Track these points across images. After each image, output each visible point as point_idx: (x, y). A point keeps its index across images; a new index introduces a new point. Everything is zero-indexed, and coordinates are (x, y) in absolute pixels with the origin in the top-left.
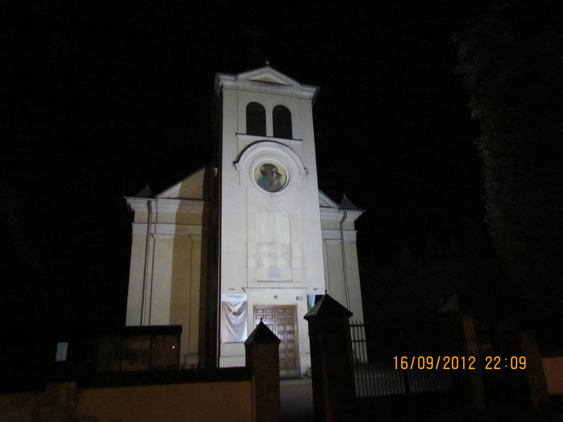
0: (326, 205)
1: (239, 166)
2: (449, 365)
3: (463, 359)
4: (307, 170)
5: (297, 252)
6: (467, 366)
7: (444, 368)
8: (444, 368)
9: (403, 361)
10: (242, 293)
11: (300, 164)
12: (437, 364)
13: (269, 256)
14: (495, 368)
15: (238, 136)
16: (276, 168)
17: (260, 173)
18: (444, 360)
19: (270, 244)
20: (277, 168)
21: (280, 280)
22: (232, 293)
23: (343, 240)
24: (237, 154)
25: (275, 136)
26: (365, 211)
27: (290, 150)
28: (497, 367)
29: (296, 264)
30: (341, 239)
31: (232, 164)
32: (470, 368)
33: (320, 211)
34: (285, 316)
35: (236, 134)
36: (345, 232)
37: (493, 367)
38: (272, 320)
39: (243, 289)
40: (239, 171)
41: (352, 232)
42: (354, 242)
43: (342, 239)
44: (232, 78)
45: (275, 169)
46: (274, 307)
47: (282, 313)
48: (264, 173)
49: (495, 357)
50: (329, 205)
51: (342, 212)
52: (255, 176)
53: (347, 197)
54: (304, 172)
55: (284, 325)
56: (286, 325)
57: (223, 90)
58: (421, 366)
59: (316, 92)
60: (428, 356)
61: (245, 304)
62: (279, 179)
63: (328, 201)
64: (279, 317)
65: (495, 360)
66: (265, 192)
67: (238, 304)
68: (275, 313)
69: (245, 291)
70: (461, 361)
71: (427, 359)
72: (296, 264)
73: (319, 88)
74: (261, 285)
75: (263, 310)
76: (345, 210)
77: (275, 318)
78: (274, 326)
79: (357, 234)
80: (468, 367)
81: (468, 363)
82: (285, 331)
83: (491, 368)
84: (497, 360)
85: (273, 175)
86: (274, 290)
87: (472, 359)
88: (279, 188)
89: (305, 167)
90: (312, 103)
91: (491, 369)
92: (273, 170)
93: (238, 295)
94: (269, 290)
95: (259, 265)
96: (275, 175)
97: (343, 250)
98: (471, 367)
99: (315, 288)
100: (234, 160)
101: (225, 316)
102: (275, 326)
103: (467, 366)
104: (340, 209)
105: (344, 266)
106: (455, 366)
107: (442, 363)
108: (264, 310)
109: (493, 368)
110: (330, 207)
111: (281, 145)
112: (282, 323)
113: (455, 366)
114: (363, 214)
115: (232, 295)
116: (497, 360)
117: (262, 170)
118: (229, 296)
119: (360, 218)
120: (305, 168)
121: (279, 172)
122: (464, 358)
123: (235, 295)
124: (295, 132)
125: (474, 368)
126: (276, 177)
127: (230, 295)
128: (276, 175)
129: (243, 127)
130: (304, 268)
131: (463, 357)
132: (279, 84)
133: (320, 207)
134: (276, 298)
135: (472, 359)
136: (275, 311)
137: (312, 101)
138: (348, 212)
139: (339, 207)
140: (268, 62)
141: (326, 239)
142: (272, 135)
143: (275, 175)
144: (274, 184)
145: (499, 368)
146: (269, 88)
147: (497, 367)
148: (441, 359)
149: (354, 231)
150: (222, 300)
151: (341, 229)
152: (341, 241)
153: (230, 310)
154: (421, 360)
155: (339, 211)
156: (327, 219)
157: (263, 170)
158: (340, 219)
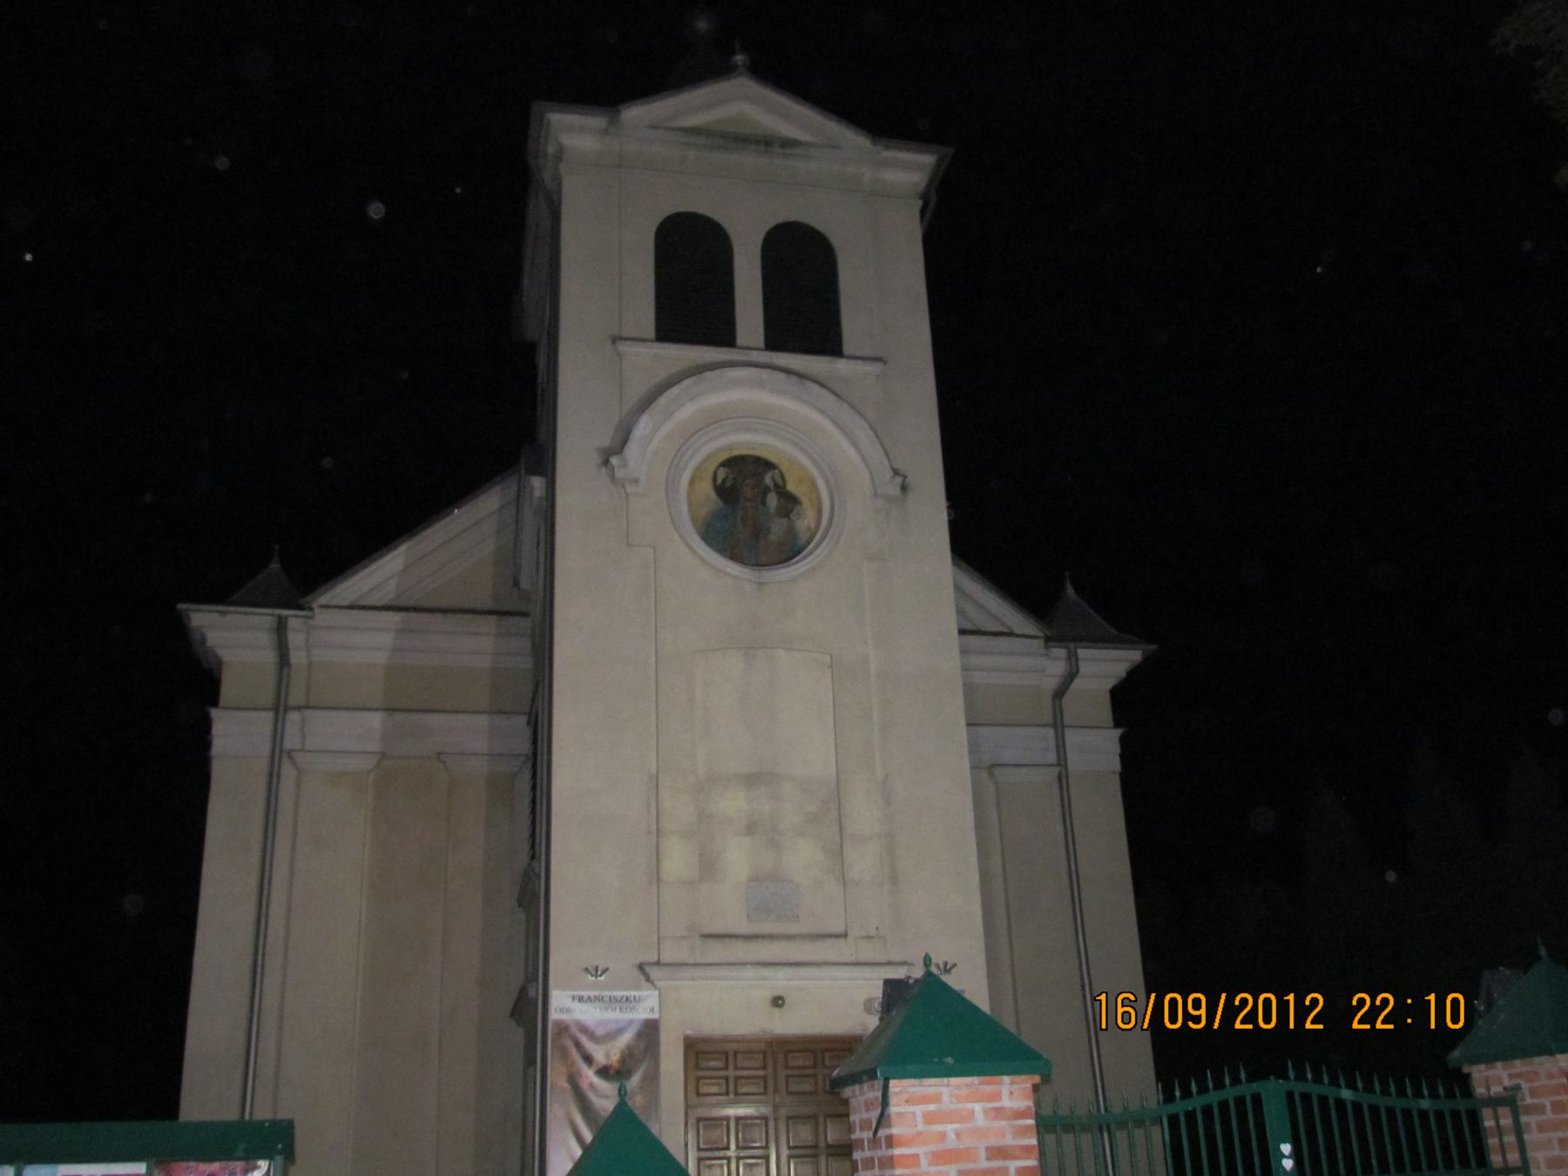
0: (991, 627)
1: (625, 464)
2: (1251, 1018)
3: (1288, 1001)
4: (905, 477)
5: (864, 814)
6: (1300, 1020)
7: (1238, 1025)
8: (1238, 1025)
9: (1123, 1006)
10: (637, 987)
11: (876, 454)
12: (1216, 1013)
13: (750, 829)
14: (1379, 1026)
15: (623, 347)
16: (776, 471)
17: (713, 495)
18: (1237, 1003)
19: (752, 780)
20: (781, 472)
21: (794, 929)
22: (594, 987)
23: (1066, 769)
24: (616, 420)
25: (776, 341)
26: (1153, 647)
27: (832, 398)
28: (1383, 1022)
29: (864, 862)
30: (1059, 765)
31: (596, 458)
32: (1308, 1026)
33: (964, 651)
34: (816, 1083)
35: (615, 339)
36: (1071, 737)
37: (1373, 1024)
38: (763, 1097)
39: (641, 967)
40: (623, 486)
41: (1101, 732)
42: (1114, 772)
43: (1063, 763)
44: (596, 121)
45: (773, 480)
46: (771, 1043)
47: (805, 1067)
48: (727, 492)
49: (1377, 996)
50: (1003, 624)
51: (1060, 652)
52: (690, 505)
53: (1077, 591)
54: (893, 490)
55: (814, 1117)
56: (821, 1119)
57: (563, 168)
58: (1173, 1020)
59: (938, 165)
60: (1192, 993)
61: (650, 1030)
62: (791, 515)
63: (995, 607)
64: (794, 1088)
65: (1378, 1003)
66: (734, 568)
67: (620, 1031)
68: (775, 1069)
69: (648, 979)
70: (1283, 1007)
71: (1190, 1000)
72: (864, 862)
73: (951, 151)
74: (717, 951)
75: (726, 1054)
76: (1071, 645)
77: (776, 1091)
78: (771, 1124)
79: (1124, 741)
80: (1305, 1023)
81: (1302, 1012)
82: (816, 1146)
83: (1368, 1027)
84: (1385, 1002)
85: (764, 503)
86: (767, 972)
87: (1315, 1002)
88: (790, 551)
89: (895, 466)
90: (923, 212)
91: (1367, 1030)
92: (763, 478)
93: (618, 994)
94: (750, 972)
95: (708, 867)
96: (772, 501)
97: (1067, 807)
98: (1312, 1023)
99: (946, 964)
100: (606, 441)
101: (564, 1084)
102: (777, 1130)
103: (1300, 1020)
104: (1049, 640)
105: (1074, 875)
106: (1267, 1020)
107: (1231, 1012)
108: (731, 1059)
109: (1373, 1025)
110: (1011, 634)
111: (795, 379)
112: (805, 1110)
113: (1267, 1020)
114: (1147, 660)
115: (597, 993)
116: (1385, 1002)
117: (719, 481)
118: (581, 999)
119: (1134, 675)
120: (896, 472)
121: (791, 487)
122: (1291, 997)
123: (607, 993)
124: (854, 326)
125: (1321, 1027)
126: (778, 508)
127: (585, 994)
128: (779, 500)
129: (642, 312)
130: (894, 880)
131: (1288, 994)
132: (788, 143)
133: (962, 632)
134: (781, 1006)
135: (1315, 1002)
136: (775, 1063)
137: (920, 203)
138: (1082, 652)
139: (1048, 633)
140: (739, 58)
141: (993, 766)
142: (761, 342)
143: (772, 501)
144: (772, 537)
145: (1391, 1027)
146: (749, 160)
147: (1383, 1022)
148: (1230, 1000)
149: (1110, 728)
150: (554, 1016)
151: (1058, 726)
152: (1057, 769)
153: (588, 1059)
154: (1173, 1002)
155: (1047, 647)
156: (540, 374)
157: (724, 480)
158: (1051, 683)
